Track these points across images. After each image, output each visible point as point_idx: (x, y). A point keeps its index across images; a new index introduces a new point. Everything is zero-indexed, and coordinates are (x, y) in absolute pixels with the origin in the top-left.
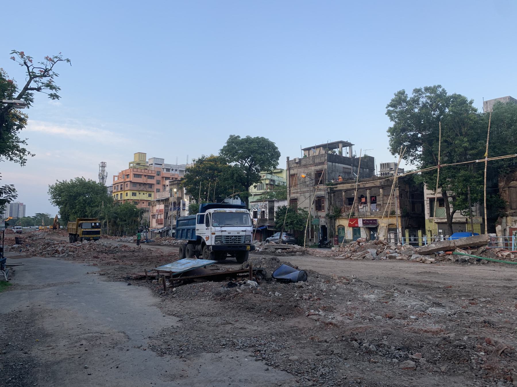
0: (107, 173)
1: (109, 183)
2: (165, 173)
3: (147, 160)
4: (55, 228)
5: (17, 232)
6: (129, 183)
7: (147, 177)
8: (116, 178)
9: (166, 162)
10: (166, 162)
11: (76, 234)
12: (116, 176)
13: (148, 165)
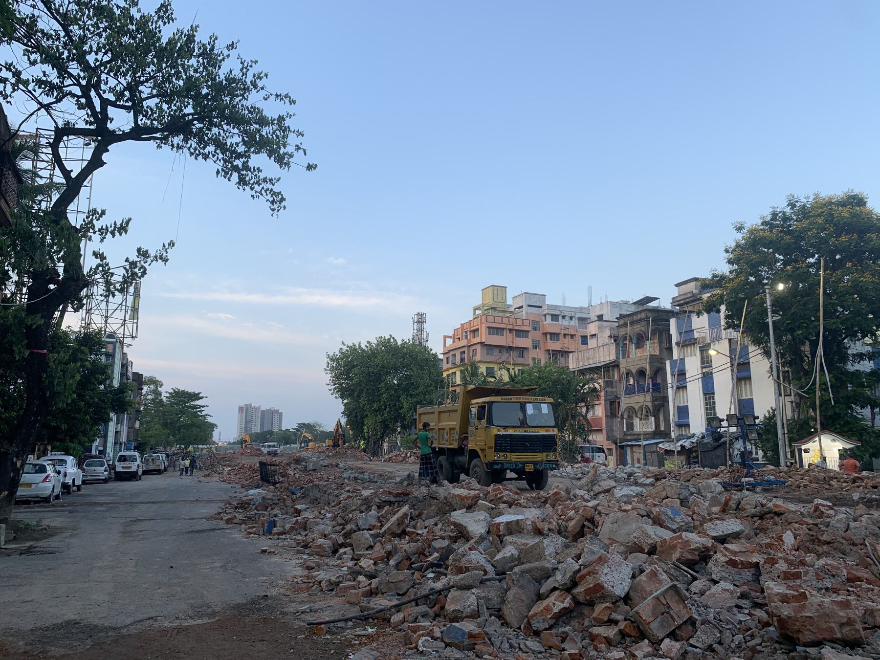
0: (428, 334)
1: (436, 347)
2: (548, 324)
3: (509, 301)
4: (336, 445)
5: (269, 453)
6: (478, 347)
7: (514, 332)
8: (449, 342)
9: (549, 301)
10: (549, 301)
11: (460, 451)
12: (450, 337)
13: (512, 309)
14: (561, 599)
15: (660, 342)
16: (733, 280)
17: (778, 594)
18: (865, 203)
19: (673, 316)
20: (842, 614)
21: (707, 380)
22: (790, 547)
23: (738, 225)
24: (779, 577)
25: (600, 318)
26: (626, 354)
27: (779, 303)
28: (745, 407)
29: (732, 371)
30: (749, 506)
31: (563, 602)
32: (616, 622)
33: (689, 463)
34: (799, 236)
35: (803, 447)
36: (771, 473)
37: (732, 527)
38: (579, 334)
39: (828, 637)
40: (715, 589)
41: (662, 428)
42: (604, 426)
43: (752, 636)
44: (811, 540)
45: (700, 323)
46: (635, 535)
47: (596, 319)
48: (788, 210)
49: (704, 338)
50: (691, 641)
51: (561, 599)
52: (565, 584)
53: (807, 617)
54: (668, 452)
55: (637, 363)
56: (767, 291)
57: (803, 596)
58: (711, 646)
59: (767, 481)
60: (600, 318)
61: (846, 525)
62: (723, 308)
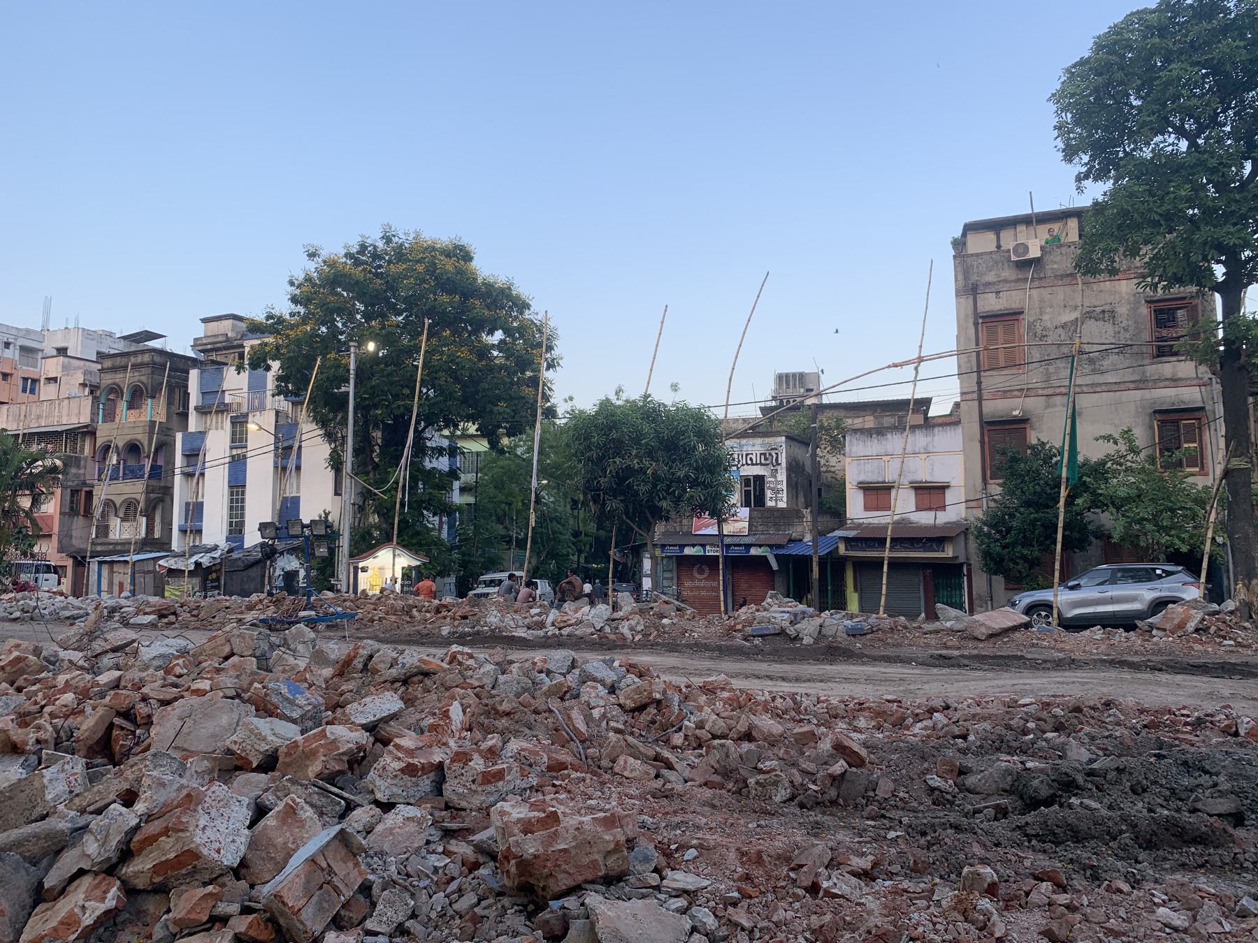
14: (98, 893)
15: (170, 403)
16: (292, 327)
17: (519, 820)
18: (471, 259)
19: (194, 367)
20: (607, 837)
21: (237, 466)
22: (459, 726)
23: (312, 250)
24: (473, 781)
25: (62, 351)
26: (110, 416)
27: (367, 367)
28: (288, 507)
29: (276, 455)
30: (382, 665)
31: (103, 900)
32: (224, 920)
33: (204, 588)
34: (392, 284)
35: (361, 565)
36: (334, 602)
37: (388, 706)
38: (19, 375)
39: (590, 877)
40: (391, 819)
41: (157, 535)
42: (56, 529)
43: (460, 891)
44: (485, 713)
45: (235, 382)
46: (234, 738)
47: (55, 353)
48: (381, 245)
49: (239, 404)
50: (370, 925)
51: (98, 893)
52: (109, 859)
53: (560, 851)
54: (171, 572)
55: (127, 431)
56: (352, 349)
57: (554, 818)
58: (401, 925)
59: (333, 614)
60: (62, 351)
61: (493, 680)
62: (276, 365)
